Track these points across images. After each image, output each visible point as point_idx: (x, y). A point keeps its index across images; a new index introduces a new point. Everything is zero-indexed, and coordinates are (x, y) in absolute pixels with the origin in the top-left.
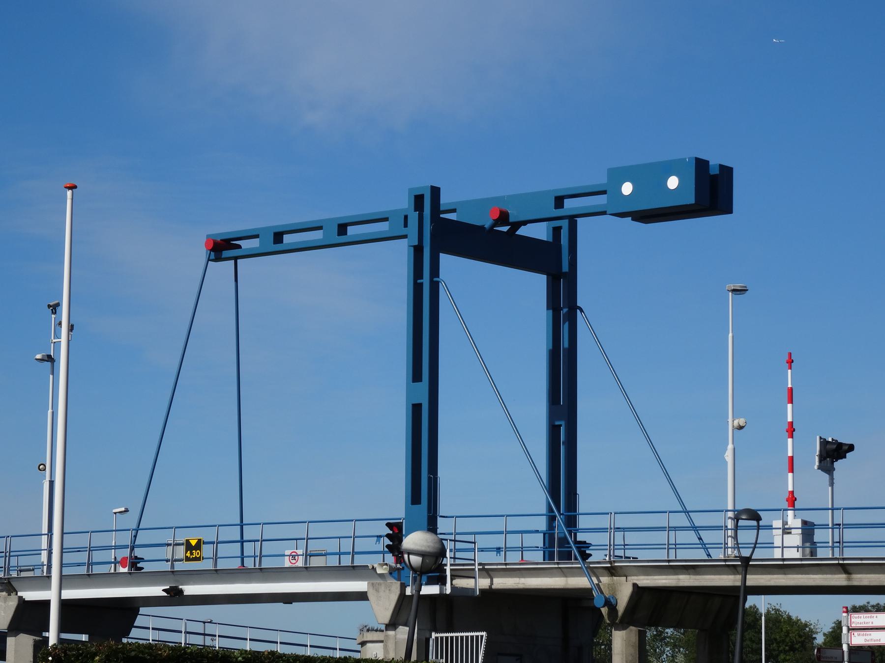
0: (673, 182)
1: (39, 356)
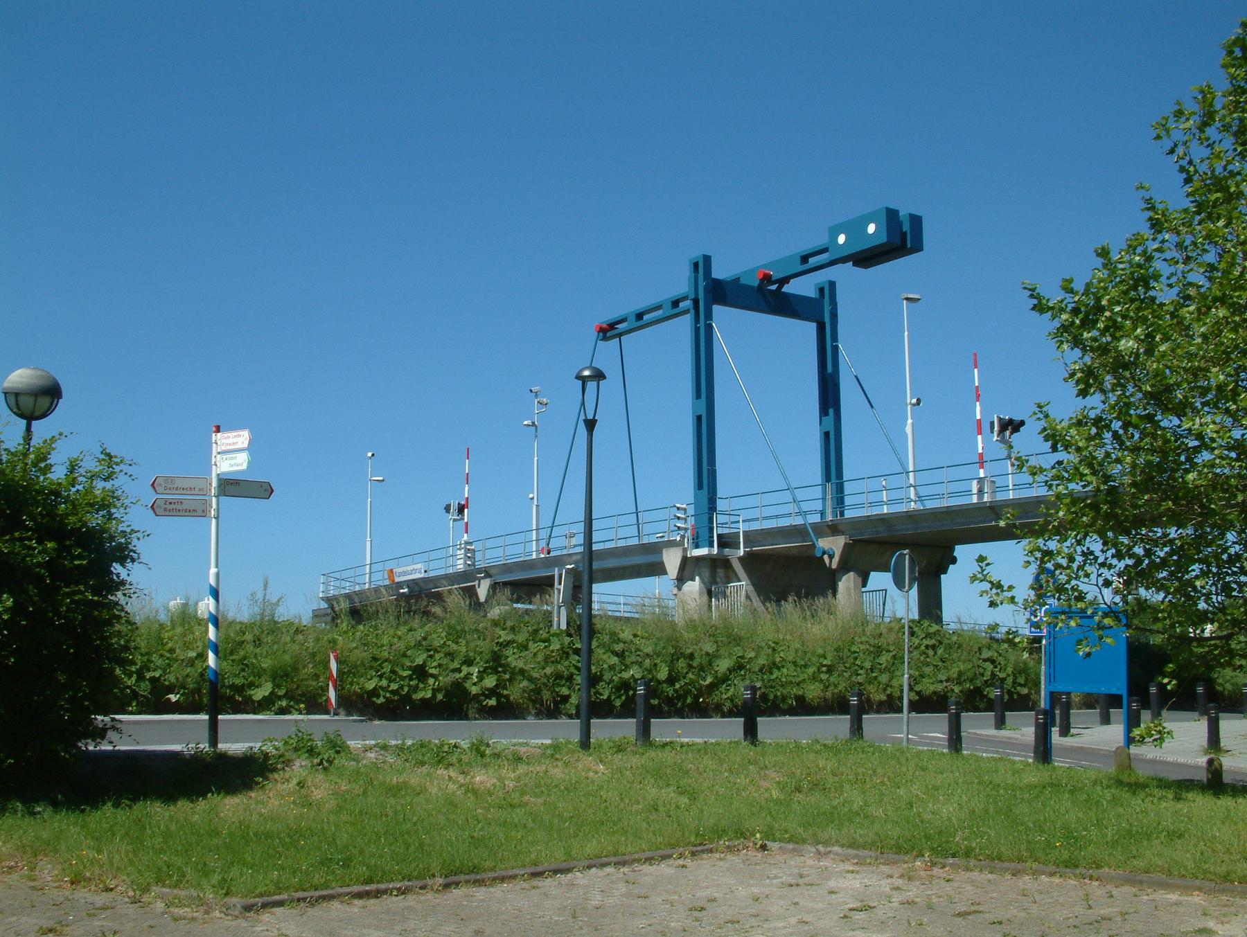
0: (871, 228)
1: (526, 423)
